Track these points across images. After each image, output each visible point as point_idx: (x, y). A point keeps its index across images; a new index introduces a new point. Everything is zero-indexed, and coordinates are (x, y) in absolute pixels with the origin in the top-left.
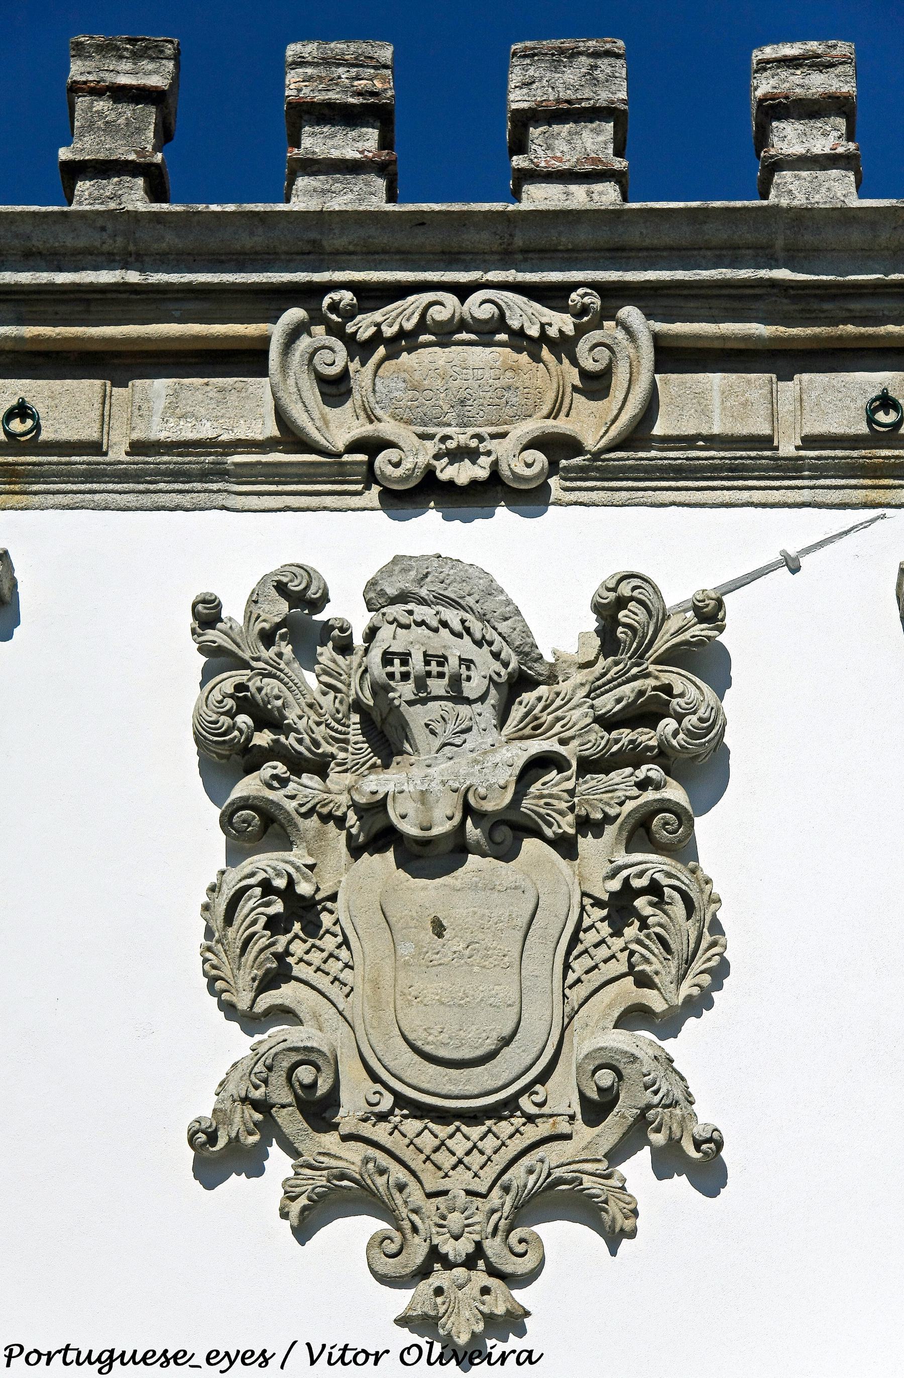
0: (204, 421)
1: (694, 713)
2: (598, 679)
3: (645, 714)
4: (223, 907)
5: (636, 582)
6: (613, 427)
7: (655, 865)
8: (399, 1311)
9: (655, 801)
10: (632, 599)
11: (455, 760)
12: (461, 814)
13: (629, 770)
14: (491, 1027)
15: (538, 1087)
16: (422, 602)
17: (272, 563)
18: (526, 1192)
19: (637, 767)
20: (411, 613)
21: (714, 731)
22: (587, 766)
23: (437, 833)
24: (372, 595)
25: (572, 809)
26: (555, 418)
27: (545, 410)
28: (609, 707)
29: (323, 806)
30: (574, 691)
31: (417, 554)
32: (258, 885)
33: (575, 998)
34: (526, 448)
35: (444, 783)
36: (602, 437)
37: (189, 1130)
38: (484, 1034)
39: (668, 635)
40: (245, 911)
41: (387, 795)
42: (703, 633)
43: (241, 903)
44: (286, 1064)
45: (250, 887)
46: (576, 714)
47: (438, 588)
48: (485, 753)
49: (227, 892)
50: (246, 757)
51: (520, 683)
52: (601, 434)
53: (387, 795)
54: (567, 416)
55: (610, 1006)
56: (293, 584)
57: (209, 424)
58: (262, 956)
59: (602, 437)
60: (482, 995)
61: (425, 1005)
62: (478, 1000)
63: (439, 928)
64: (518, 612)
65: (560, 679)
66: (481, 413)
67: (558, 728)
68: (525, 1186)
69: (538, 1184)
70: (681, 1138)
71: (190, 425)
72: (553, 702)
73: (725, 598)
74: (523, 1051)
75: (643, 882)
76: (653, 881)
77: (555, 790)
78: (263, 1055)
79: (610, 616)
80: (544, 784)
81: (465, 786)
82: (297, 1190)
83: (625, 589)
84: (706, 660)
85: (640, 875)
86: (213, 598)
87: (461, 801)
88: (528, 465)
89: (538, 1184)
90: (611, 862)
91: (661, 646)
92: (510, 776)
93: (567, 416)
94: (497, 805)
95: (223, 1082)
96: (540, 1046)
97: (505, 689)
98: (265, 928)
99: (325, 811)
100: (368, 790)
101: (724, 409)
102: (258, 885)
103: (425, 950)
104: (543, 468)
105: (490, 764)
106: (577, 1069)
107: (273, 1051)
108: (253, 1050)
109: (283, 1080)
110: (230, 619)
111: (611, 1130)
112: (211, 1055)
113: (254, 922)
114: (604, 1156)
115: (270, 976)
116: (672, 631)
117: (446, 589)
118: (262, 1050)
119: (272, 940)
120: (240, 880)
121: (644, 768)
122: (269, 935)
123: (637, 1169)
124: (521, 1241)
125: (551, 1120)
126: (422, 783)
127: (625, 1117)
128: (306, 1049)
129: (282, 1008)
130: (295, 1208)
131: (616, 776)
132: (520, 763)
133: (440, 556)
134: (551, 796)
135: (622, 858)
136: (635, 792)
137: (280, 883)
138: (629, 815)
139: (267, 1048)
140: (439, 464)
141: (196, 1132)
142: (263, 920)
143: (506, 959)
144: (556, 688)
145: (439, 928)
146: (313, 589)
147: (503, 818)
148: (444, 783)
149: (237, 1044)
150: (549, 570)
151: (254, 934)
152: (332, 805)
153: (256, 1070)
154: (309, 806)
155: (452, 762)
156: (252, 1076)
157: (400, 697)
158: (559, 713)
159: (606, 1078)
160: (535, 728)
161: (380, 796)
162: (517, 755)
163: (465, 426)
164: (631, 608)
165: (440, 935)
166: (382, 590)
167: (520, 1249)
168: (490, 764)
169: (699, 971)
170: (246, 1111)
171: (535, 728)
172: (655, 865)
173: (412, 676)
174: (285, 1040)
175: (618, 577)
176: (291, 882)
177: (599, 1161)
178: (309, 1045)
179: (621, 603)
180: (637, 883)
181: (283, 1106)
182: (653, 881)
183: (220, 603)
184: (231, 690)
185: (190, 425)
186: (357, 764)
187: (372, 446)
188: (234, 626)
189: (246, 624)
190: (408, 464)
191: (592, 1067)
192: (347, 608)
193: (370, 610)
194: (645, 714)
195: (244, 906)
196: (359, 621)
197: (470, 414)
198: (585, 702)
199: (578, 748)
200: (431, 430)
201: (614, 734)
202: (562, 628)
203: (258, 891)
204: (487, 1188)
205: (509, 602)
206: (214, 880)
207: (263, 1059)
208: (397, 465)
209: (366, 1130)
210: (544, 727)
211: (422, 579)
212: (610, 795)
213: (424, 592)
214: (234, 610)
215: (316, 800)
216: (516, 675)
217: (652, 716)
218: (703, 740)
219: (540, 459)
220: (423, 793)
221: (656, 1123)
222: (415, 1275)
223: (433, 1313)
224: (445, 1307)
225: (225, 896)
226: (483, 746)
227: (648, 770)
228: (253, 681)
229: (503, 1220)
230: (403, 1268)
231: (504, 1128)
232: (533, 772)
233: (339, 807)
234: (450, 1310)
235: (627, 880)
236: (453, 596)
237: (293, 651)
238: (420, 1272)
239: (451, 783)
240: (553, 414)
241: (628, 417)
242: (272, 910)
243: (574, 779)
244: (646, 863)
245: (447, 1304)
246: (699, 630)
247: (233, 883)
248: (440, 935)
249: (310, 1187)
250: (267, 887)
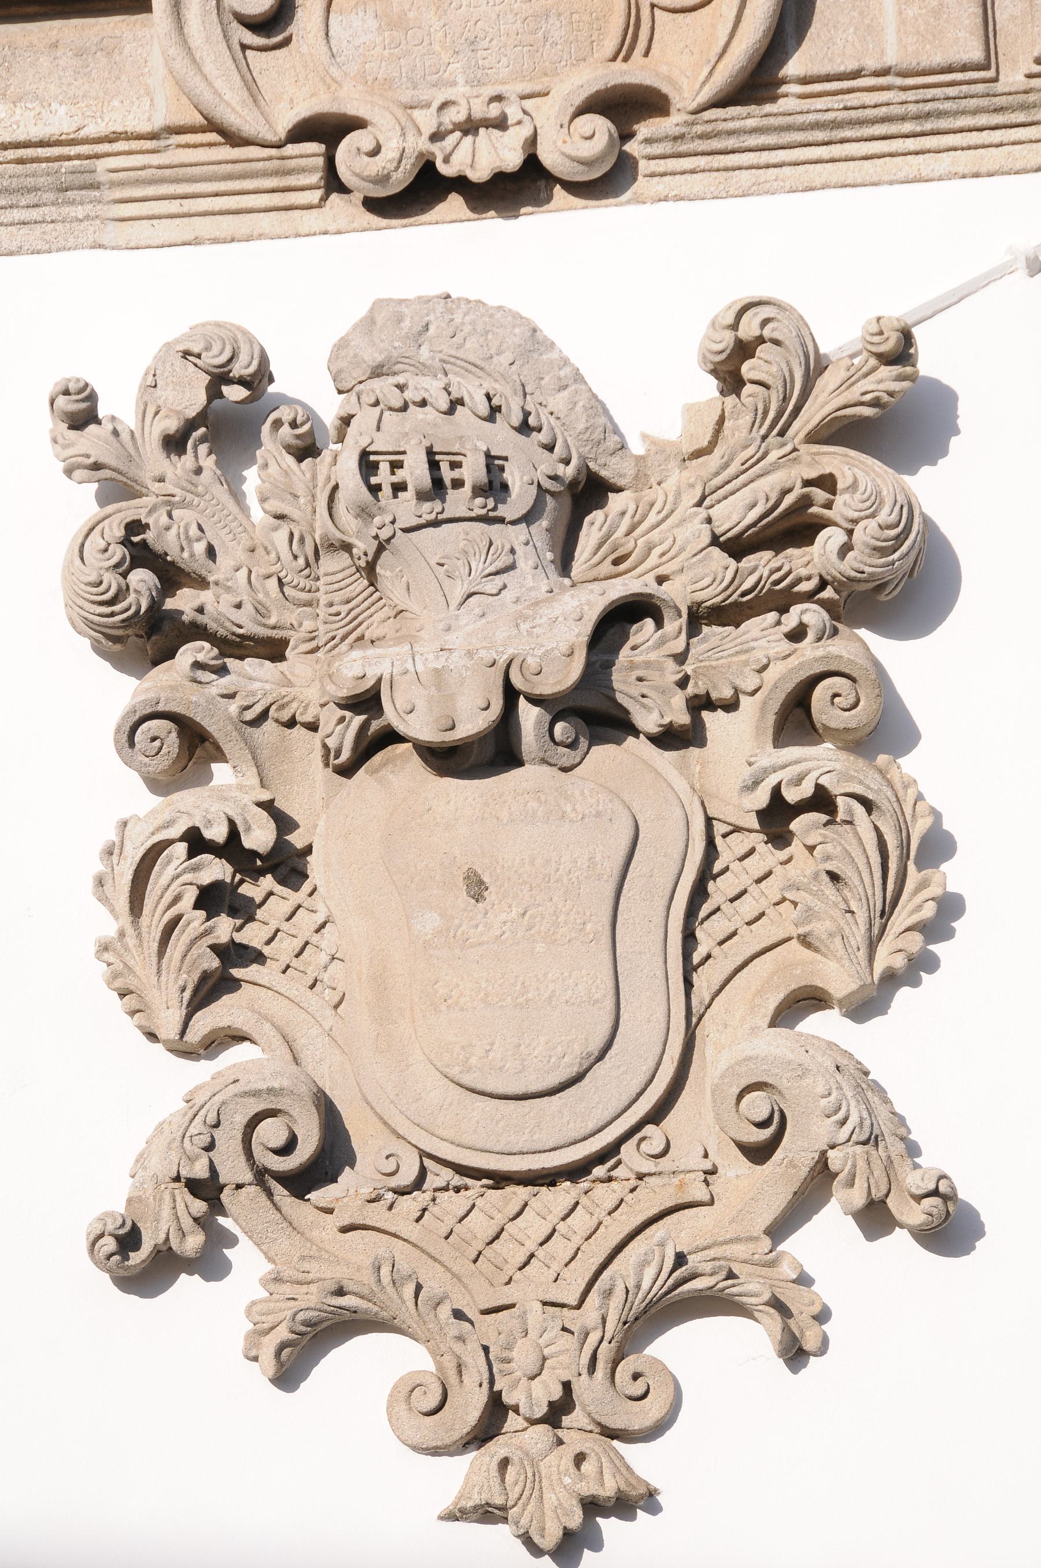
0: (55, 106)
1: (873, 516)
2: (717, 474)
3: (794, 527)
4: (129, 876)
5: (765, 312)
6: (721, 66)
7: (821, 763)
8: (446, 1502)
9: (816, 660)
10: (761, 340)
11: (490, 617)
12: (501, 702)
13: (772, 616)
14: (569, 1038)
15: (649, 1129)
16: (423, 369)
17: (176, 326)
18: (640, 1296)
19: (784, 610)
20: (401, 388)
21: (908, 543)
22: (699, 618)
23: (464, 735)
24: (341, 364)
25: (683, 683)
26: (626, 59)
27: (610, 44)
28: (735, 518)
29: (282, 707)
30: (678, 494)
31: (411, 295)
32: (182, 839)
33: (705, 984)
34: (580, 112)
35: (470, 654)
36: (704, 83)
37: (89, 1234)
38: (559, 1049)
39: (826, 394)
40: (164, 880)
41: (379, 680)
42: (881, 387)
43: (156, 868)
44: (241, 1119)
45: (169, 843)
46: (683, 534)
47: (447, 348)
48: (537, 603)
49: (133, 854)
50: (153, 638)
51: (589, 492)
52: (702, 78)
53: (379, 680)
54: (646, 54)
55: (760, 992)
56: (211, 354)
57: (62, 110)
58: (194, 952)
59: (704, 83)
60: (551, 986)
61: (462, 1010)
62: (546, 995)
63: (477, 887)
64: (578, 377)
65: (653, 481)
66: (504, 60)
67: (653, 559)
68: (638, 1287)
69: (659, 1283)
70: (887, 1195)
71: (32, 113)
72: (644, 517)
73: (915, 331)
74: (625, 1072)
75: (807, 790)
76: (819, 789)
77: (653, 656)
78: (202, 1107)
79: (730, 373)
80: (634, 648)
81: (505, 657)
82: (270, 1318)
83: (749, 328)
84: (901, 422)
85: (798, 781)
86: (82, 384)
87: (500, 682)
88: (576, 144)
89: (659, 1283)
90: (750, 764)
91: (813, 414)
92: (578, 636)
93: (646, 54)
94: (559, 682)
95: (141, 1155)
96: (651, 1064)
97: (567, 501)
98: (197, 906)
99: (285, 716)
100: (350, 675)
101: (903, 22)
102: (182, 839)
103: (457, 921)
104: (611, 135)
105: (544, 620)
106: (713, 1092)
107: (218, 1099)
108: (188, 1102)
109: (236, 1144)
110: (113, 418)
111: (774, 1183)
112: (127, 1105)
113: (177, 899)
114: (765, 1232)
115: (210, 983)
116: (832, 387)
117: (459, 347)
118: (198, 1101)
119: (208, 923)
120: (153, 834)
121: (796, 610)
122: (223, 899)
123: (828, 1240)
124: (636, 1377)
125: (675, 1181)
126: (437, 658)
127: (795, 1167)
128: (270, 1091)
129: (230, 1033)
130: (269, 1345)
131: (754, 626)
132: (592, 616)
133: (448, 297)
134: (648, 665)
135: (772, 756)
136: (786, 646)
137: (217, 833)
138: (775, 686)
139: (209, 1094)
140: (438, 151)
141: (101, 1236)
142: (191, 895)
143: (589, 926)
144: (648, 495)
145: (477, 887)
146: (243, 358)
147: (571, 704)
148: (470, 654)
149: (173, 1084)
150: (620, 310)
151: (178, 918)
152: (295, 705)
153: (193, 1130)
154: (258, 709)
155: (483, 621)
156: (187, 1140)
157: (393, 522)
158: (655, 535)
159: (758, 1105)
160: (616, 562)
161: (369, 683)
162: (589, 603)
163: (480, 83)
164: (762, 355)
165: (478, 898)
166: (356, 356)
167: (638, 1388)
168: (544, 620)
169: (903, 928)
170: (179, 1199)
171: (616, 562)
172: (821, 763)
173: (410, 487)
174: (236, 1081)
175: (738, 307)
176: (234, 834)
177: (752, 1239)
178: (276, 1085)
179: (744, 350)
180: (792, 795)
181: (239, 1187)
182: (819, 789)
183: (93, 391)
184: (120, 533)
185: (32, 113)
186: (333, 638)
187: (327, 130)
188: (119, 428)
189: (140, 424)
190: (390, 153)
191: (736, 1091)
192: (304, 381)
193: (340, 392)
194: (794, 527)
195: (160, 874)
196: (328, 408)
197: (486, 63)
198: (696, 514)
199: (689, 589)
200: (424, 95)
201: (749, 561)
202: (650, 392)
203: (182, 848)
204: (578, 1295)
205: (566, 362)
206: (113, 836)
207: (202, 1113)
208: (375, 152)
209: (376, 1215)
210: (631, 559)
211: (420, 334)
212: (743, 657)
213: (425, 354)
214: (118, 404)
215: (270, 700)
216: (583, 478)
217: (829, 508)
218: (891, 558)
219: (600, 126)
220: (438, 673)
221: (846, 1171)
222: (468, 1443)
223: (499, 1501)
224: (518, 1489)
225: (129, 860)
226: (533, 594)
227: (802, 613)
228: (155, 515)
229: (605, 1344)
230: (447, 1432)
231: (605, 1195)
232: (613, 631)
233: (306, 708)
234: (526, 1493)
235: (776, 793)
236: (471, 358)
237: (217, 463)
238: (475, 1438)
239: (483, 653)
240: (624, 51)
241: (744, 46)
242: (206, 877)
243: (683, 636)
244: (805, 760)
245: (521, 1484)
246: (884, 380)
247: (142, 838)
248: (478, 898)
249: (289, 1314)
250: (196, 842)
